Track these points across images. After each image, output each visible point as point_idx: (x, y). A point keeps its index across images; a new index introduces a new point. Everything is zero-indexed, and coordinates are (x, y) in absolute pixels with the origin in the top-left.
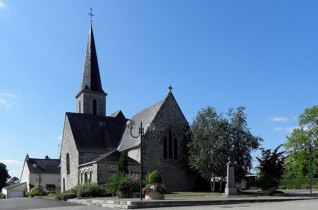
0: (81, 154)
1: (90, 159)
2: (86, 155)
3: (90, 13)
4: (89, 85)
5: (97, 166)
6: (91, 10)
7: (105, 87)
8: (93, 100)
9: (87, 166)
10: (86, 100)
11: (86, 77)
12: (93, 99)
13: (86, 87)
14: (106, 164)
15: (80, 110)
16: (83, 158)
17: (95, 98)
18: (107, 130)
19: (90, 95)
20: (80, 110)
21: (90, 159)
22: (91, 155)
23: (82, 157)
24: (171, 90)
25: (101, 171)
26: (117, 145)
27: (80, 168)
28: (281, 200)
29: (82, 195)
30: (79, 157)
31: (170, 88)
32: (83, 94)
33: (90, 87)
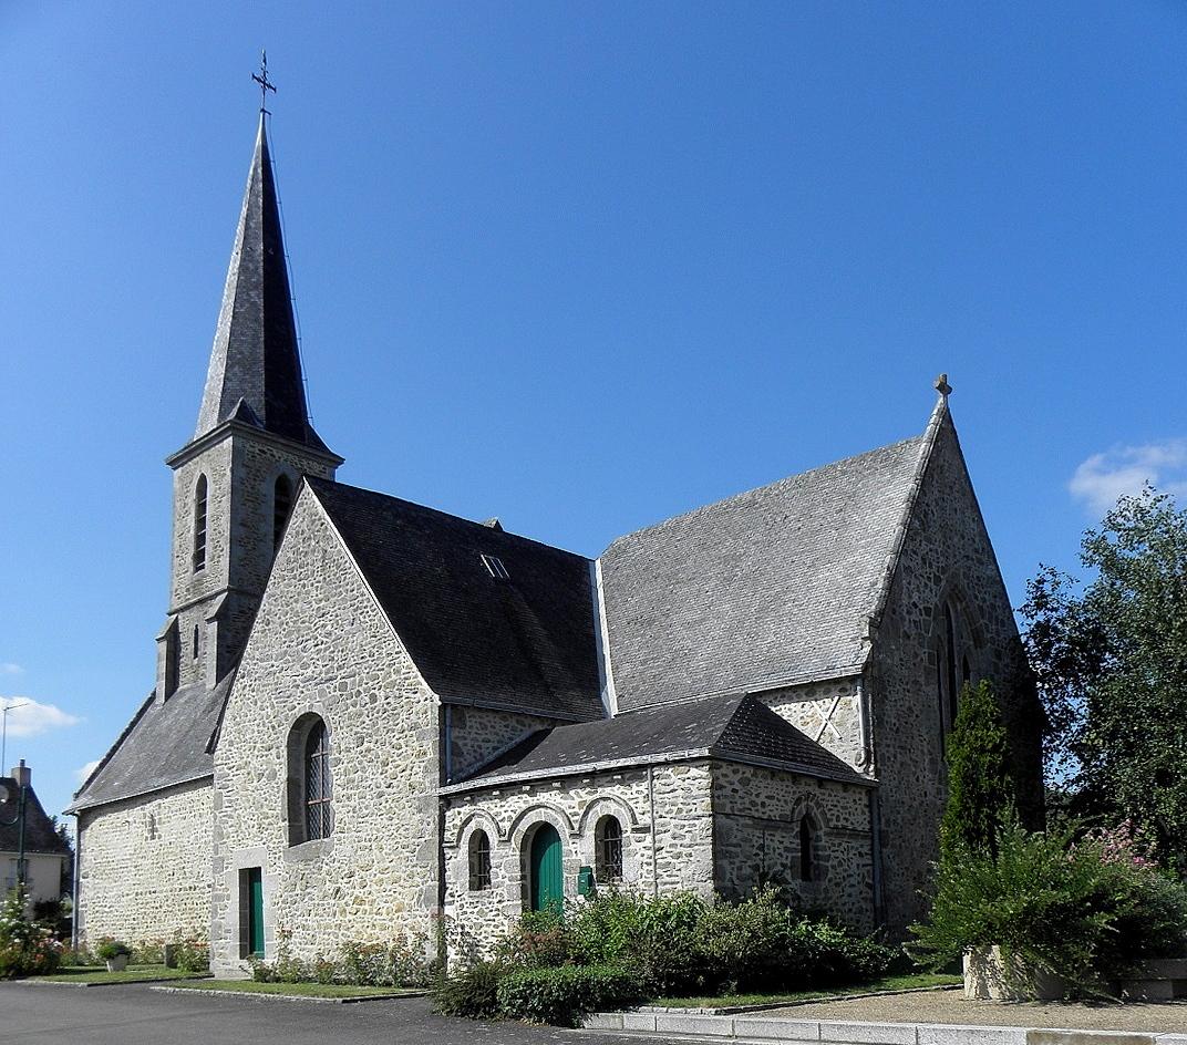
0: (450, 715)
1: (495, 749)
2: (472, 721)
3: (259, 74)
4: (258, 404)
5: (705, 783)
6: (265, 61)
7: (321, 419)
8: (276, 477)
9: (563, 789)
10: (242, 472)
11: (239, 363)
12: (280, 473)
13: (244, 413)
14: (748, 775)
15: (201, 523)
16: (460, 743)
17: (287, 472)
18: (520, 596)
19: (264, 452)
20: (201, 523)
21: (495, 749)
22: (499, 723)
23: (456, 733)
24: (945, 396)
25: (727, 815)
26: (589, 678)
27: (447, 802)
28: (66, 869)
29: (670, 977)
30: (442, 733)
31: (944, 388)
32: (231, 438)
33: (261, 413)
